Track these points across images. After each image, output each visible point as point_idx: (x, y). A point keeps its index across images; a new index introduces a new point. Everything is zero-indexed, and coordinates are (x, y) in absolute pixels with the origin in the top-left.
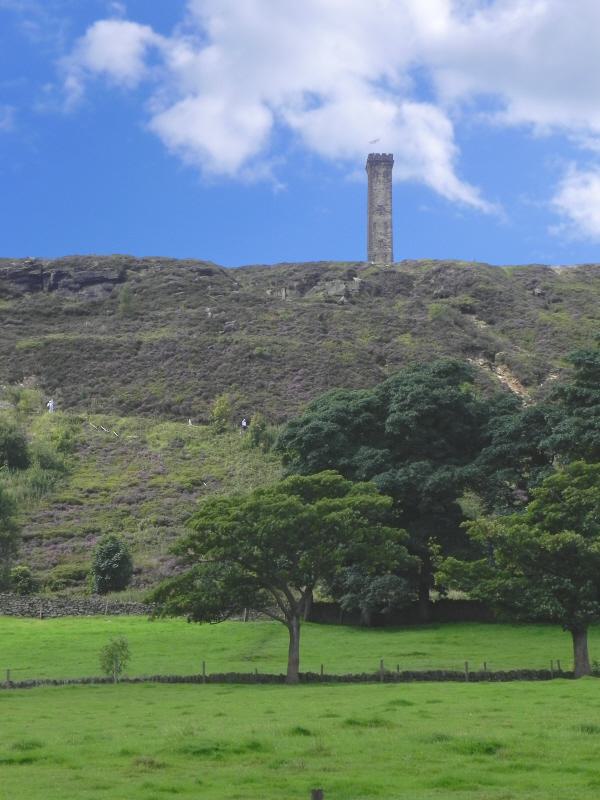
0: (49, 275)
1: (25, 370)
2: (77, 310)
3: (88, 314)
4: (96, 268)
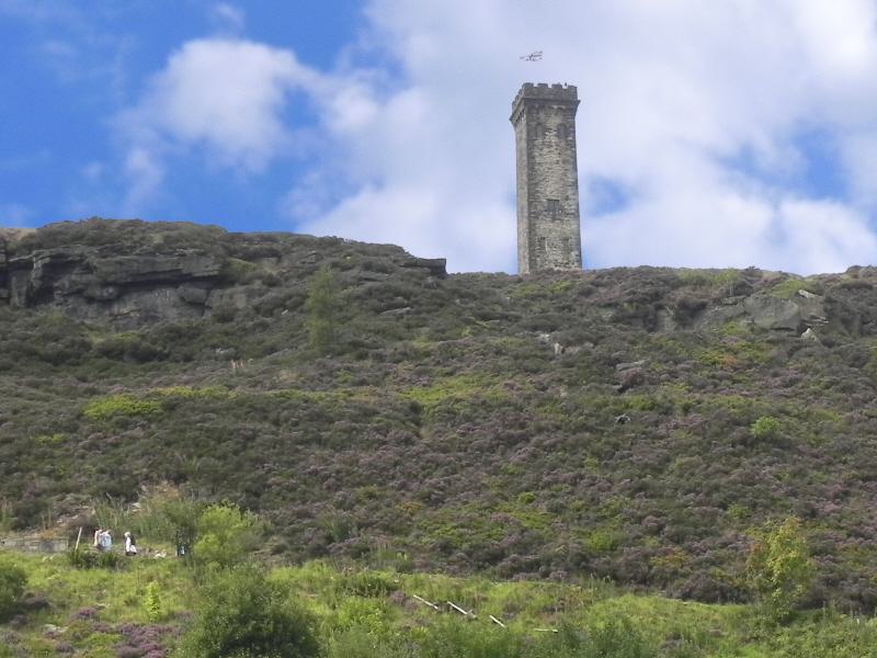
0: (28, 266)
1: (139, 467)
2: (136, 347)
3: (163, 357)
4: (158, 248)
